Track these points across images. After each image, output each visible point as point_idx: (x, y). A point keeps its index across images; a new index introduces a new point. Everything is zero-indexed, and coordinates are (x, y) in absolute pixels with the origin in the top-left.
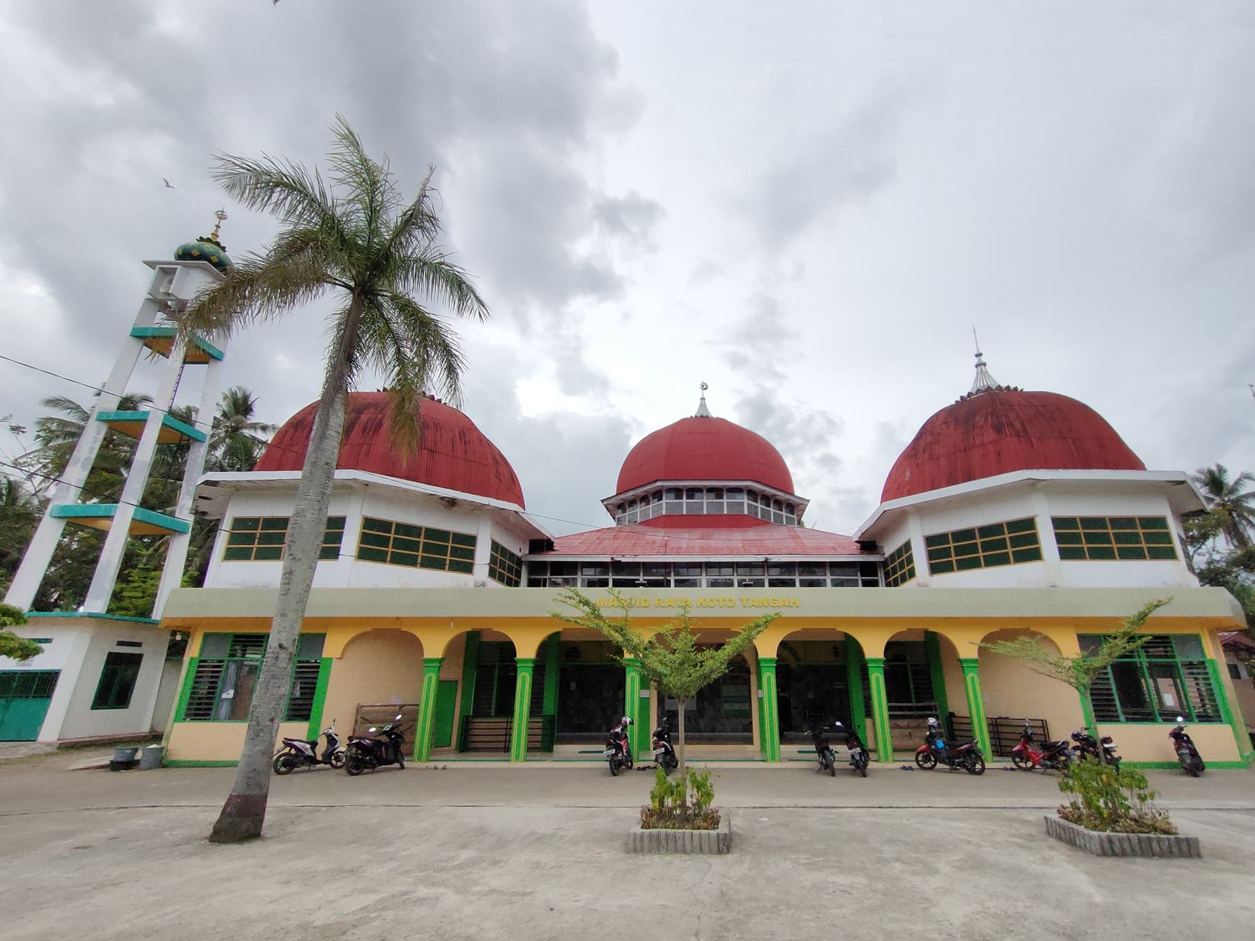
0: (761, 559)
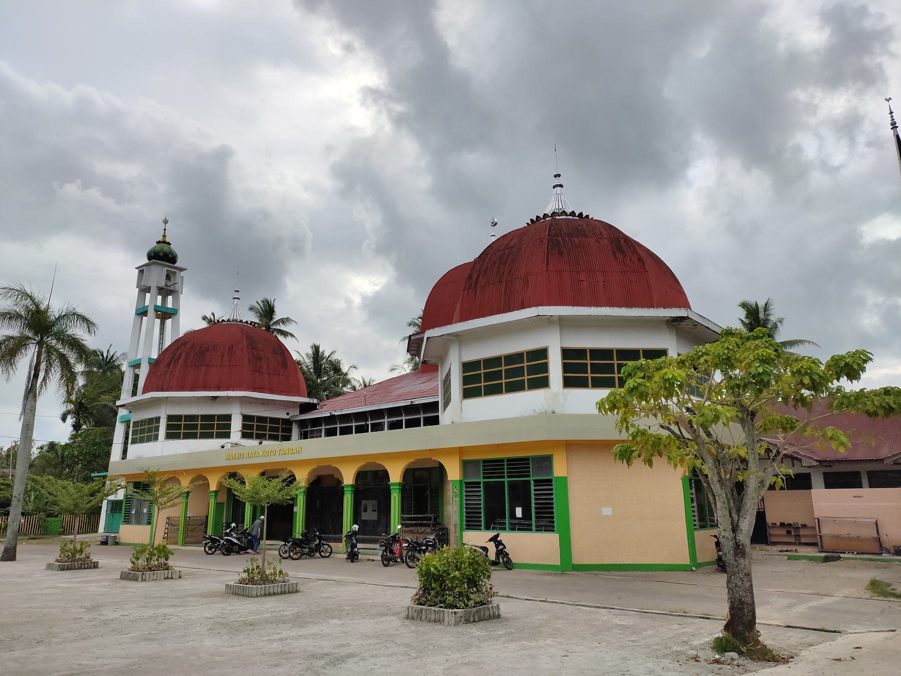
0: (408, 403)
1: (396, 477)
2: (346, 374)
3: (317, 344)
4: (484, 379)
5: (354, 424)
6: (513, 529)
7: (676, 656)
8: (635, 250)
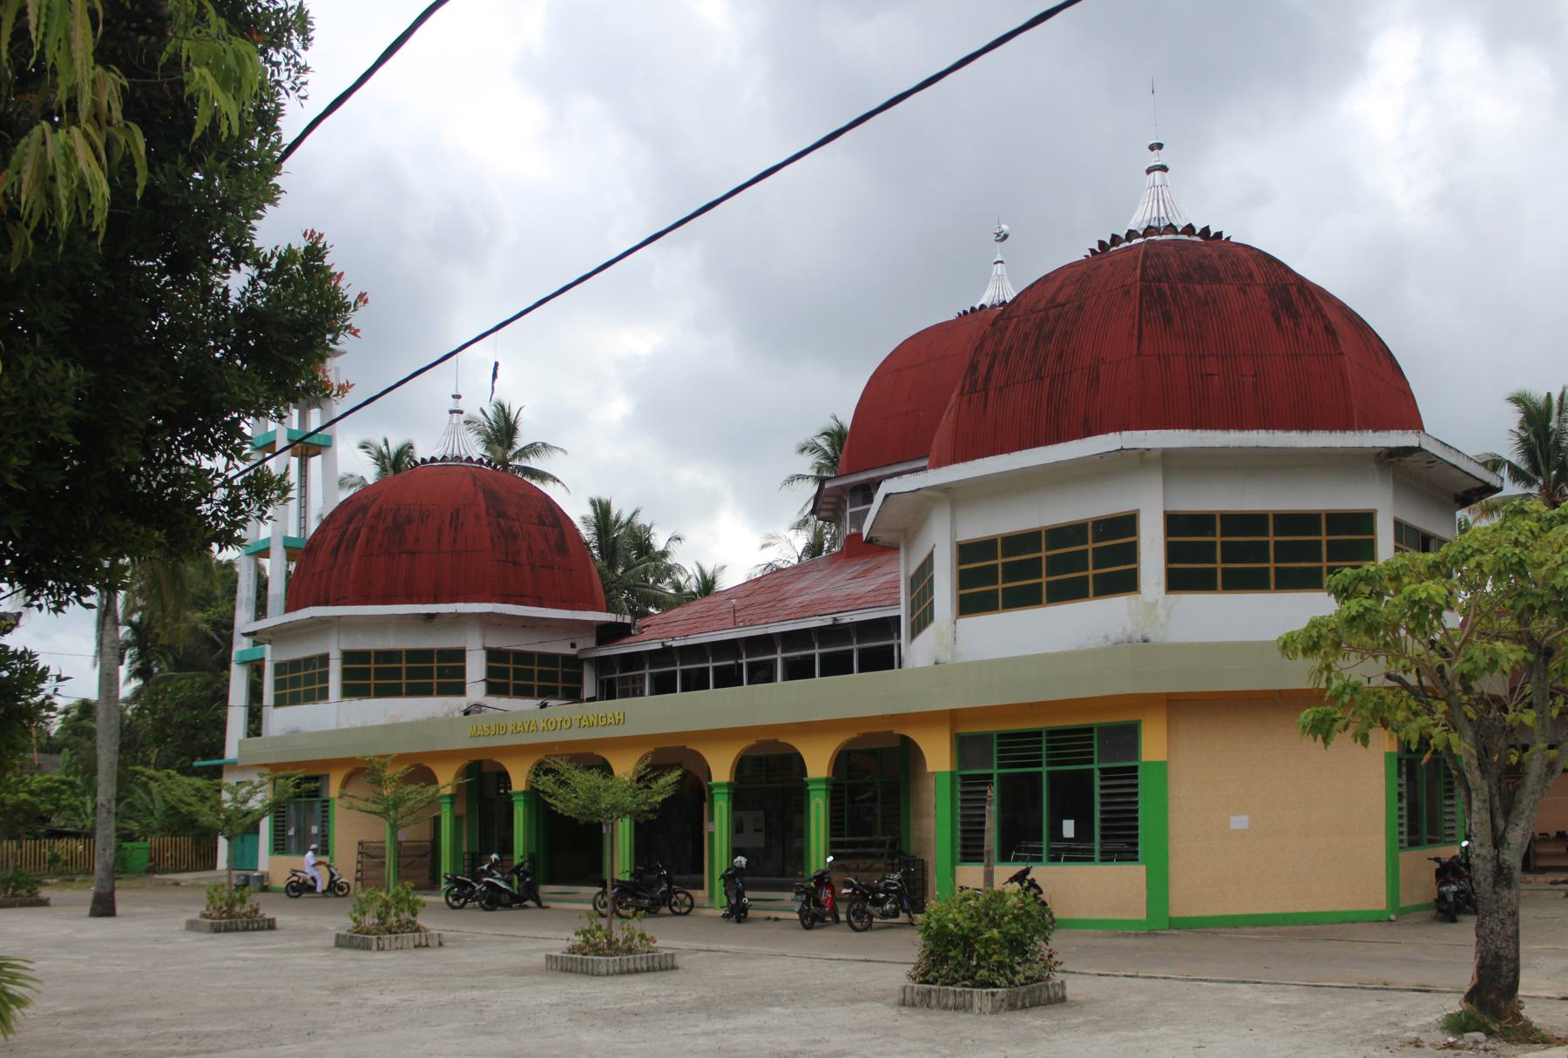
1: (818, 763)
2: (664, 554)
3: (605, 497)
4: (1005, 575)
5: (711, 665)
6: (1055, 859)
7: (1384, 1042)
8: (1320, 309)
